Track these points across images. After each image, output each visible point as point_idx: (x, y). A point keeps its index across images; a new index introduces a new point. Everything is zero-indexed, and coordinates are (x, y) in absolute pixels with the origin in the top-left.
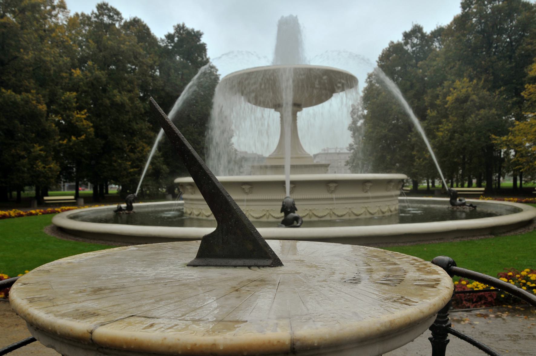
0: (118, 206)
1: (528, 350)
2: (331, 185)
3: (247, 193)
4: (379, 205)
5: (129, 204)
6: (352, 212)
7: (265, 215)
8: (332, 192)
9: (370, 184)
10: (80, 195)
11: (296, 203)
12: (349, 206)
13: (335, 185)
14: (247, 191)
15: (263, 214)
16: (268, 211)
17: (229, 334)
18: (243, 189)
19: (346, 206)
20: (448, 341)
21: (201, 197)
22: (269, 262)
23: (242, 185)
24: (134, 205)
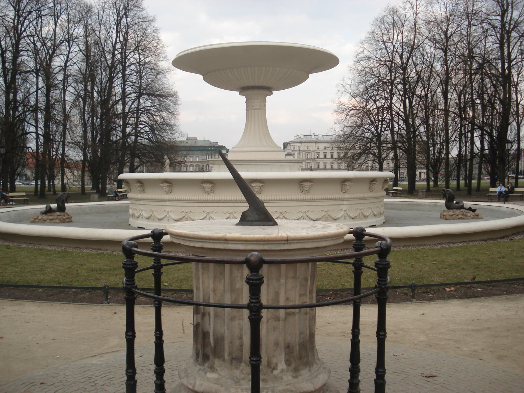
0: (46, 207)
1: (40, 250)
2: (305, 184)
3: (208, 193)
4: (134, 208)
5: (61, 205)
6: (329, 215)
7: (184, 217)
8: (307, 192)
9: (350, 183)
10: (461, 188)
12: (305, 209)
13: (309, 184)
15: (182, 216)
16: (281, 213)
17: (487, 286)
18: (204, 187)
19: (300, 209)
20: (362, 272)
21: (243, 198)
22: (272, 223)
23: (202, 183)
24: (66, 205)
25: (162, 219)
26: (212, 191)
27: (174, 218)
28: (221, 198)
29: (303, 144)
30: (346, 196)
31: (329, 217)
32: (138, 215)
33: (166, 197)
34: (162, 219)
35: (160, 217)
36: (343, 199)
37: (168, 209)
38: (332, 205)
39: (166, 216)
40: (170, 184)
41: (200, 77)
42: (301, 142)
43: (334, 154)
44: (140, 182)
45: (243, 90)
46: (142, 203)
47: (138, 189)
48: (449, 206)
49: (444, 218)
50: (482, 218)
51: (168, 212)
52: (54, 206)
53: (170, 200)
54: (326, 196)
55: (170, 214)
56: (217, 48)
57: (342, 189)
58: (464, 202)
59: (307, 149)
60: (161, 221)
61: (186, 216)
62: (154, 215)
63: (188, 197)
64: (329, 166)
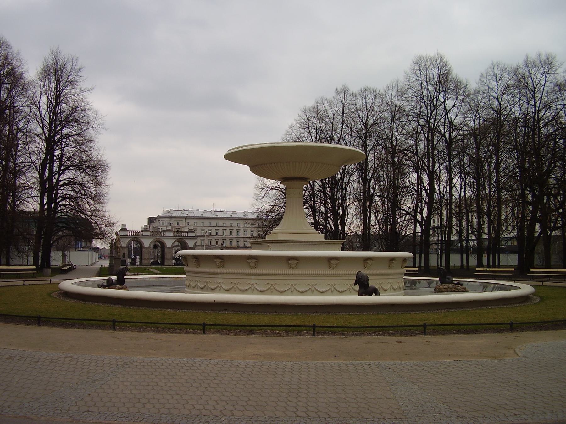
2: (333, 261)
6: (335, 288)
8: (334, 269)
11: (369, 278)
12: (332, 282)
13: (336, 262)
14: (293, 266)
18: (250, 262)
25: (215, 289)
26: (255, 267)
27: (260, 290)
28: (281, 272)
29: (173, 220)
30: (252, 271)
31: (334, 290)
32: (194, 285)
33: (252, 271)
34: (215, 289)
35: (212, 287)
36: (390, 274)
37: (253, 282)
38: (259, 279)
39: (218, 286)
40: (223, 260)
41: (247, 168)
42: (171, 217)
43: (248, 231)
44: (197, 258)
45: (284, 180)
46: (220, 276)
47: (194, 264)
48: (442, 281)
49: (438, 291)
50: (468, 291)
51: (220, 283)
52: (114, 278)
53: (222, 273)
54: (344, 272)
55: (208, 284)
56: (344, 149)
57: (389, 266)
58: (454, 279)
59: (176, 225)
60: (386, 291)
61: (235, 287)
62: (208, 286)
63: (241, 271)
64: (249, 244)
